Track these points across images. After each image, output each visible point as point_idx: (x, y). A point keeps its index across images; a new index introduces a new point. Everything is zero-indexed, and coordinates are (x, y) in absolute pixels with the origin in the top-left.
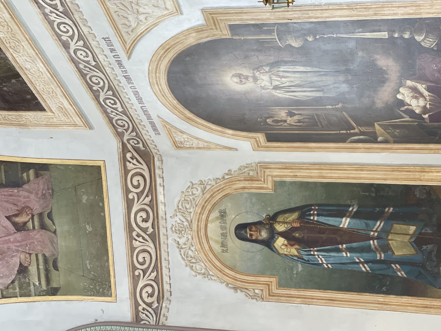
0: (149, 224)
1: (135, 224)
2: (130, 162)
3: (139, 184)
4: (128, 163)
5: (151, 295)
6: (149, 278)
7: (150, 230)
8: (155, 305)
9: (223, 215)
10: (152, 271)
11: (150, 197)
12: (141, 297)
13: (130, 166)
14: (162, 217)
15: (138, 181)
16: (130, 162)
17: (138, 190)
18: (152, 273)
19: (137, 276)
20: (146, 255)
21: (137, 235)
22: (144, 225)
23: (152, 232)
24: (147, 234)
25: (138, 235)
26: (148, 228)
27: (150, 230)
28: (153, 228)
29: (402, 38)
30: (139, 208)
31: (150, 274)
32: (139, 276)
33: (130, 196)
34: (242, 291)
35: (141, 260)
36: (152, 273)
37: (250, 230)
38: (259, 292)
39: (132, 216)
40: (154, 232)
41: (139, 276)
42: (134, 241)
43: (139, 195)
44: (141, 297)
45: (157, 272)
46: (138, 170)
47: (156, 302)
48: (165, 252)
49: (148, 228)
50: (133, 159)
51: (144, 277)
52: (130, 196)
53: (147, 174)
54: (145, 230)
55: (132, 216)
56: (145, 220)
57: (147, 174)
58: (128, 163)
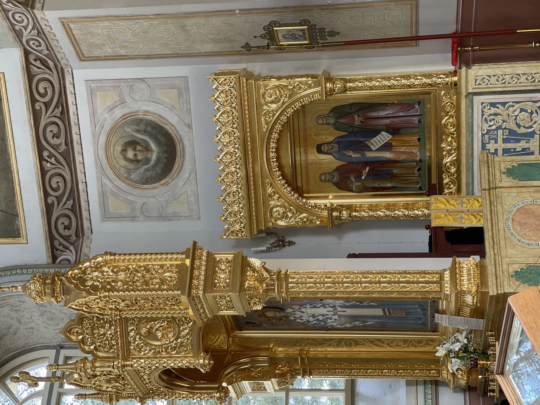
0: (62, 140)
2: (47, 162)
3: (59, 187)
4: (44, 162)
5: (67, 228)
10: (68, 199)
11: (60, 108)
12: (48, 142)
15: (58, 182)
17: (46, 99)
18: (68, 202)
19: (51, 204)
20: (60, 179)
21: (48, 156)
23: (65, 150)
24: (59, 153)
26: (70, 236)
27: (63, 147)
30: (60, 213)
31: (65, 203)
32: (53, 203)
33: (50, 201)
36: (68, 202)
39: (30, 20)
41: (53, 203)
42: (32, 66)
43: (59, 199)
44: (48, 142)
45: (74, 201)
46: (57, 171)
48: (81, 173)
49: (70, 236)
51: (58, 205)
52: (37, 108)
53: (68, 177)
54: (55, 147)
55: (30, 20)
57: (68, 177)
58: (44, 162)
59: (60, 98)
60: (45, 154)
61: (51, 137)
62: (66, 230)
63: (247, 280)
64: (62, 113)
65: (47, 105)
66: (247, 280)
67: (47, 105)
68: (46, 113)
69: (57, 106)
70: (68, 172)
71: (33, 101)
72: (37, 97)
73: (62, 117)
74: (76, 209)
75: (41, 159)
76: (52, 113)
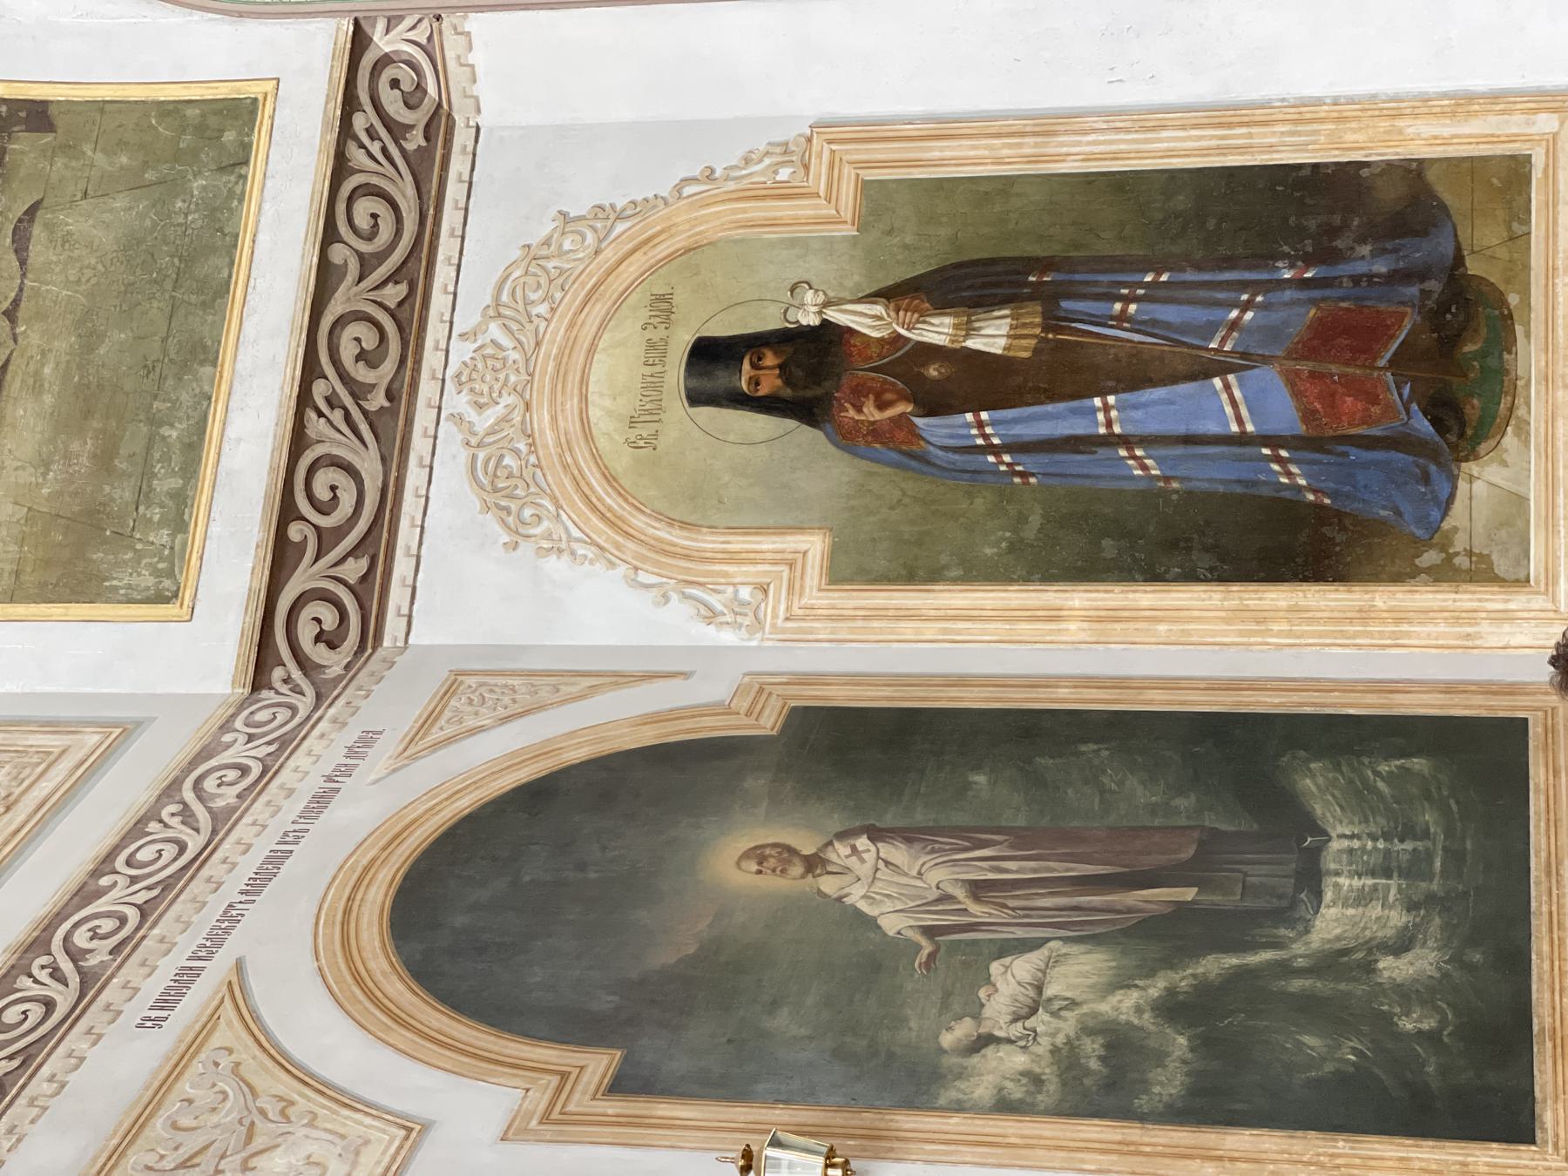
1: (306, 502)
2: (320, 414)
5: (368, 358)
6: (411, 35)
7: (377, 401)
8: (415, 141)
9: (663, 306)
10: (353, 552)
13: (357, 157)
14: (421, 459)
16: (320, 414)
22: (361, 373)
24: (365, 413)
25: (332, 401)
28: (427, 138)
29: (1375, 848)
33: (295, 532)
34: (686, 597)
35: (363, 222)
37: (754, 366)
38: (752, 595)
40: (425, 154)
42: (313, 415)
47: (382, 393)
50: (332, 407)
52: (295, 532)
56: (368, 358)
59: (377, 529)
60: (319, 390)
61: (352, 359)
62: (361, 364)
63: (1329, 873)
64: (366, 578)
65: (367, 264)
66: (1329, 873)
67: (326, 539)
68: (316, 561)
69: (393, 278)
70: (410, 190)
71: (287, 512)
72: (343, 228)
73: (403, 314)
74: (409, 321)
75: (304, 399)
76: (335, 565)
